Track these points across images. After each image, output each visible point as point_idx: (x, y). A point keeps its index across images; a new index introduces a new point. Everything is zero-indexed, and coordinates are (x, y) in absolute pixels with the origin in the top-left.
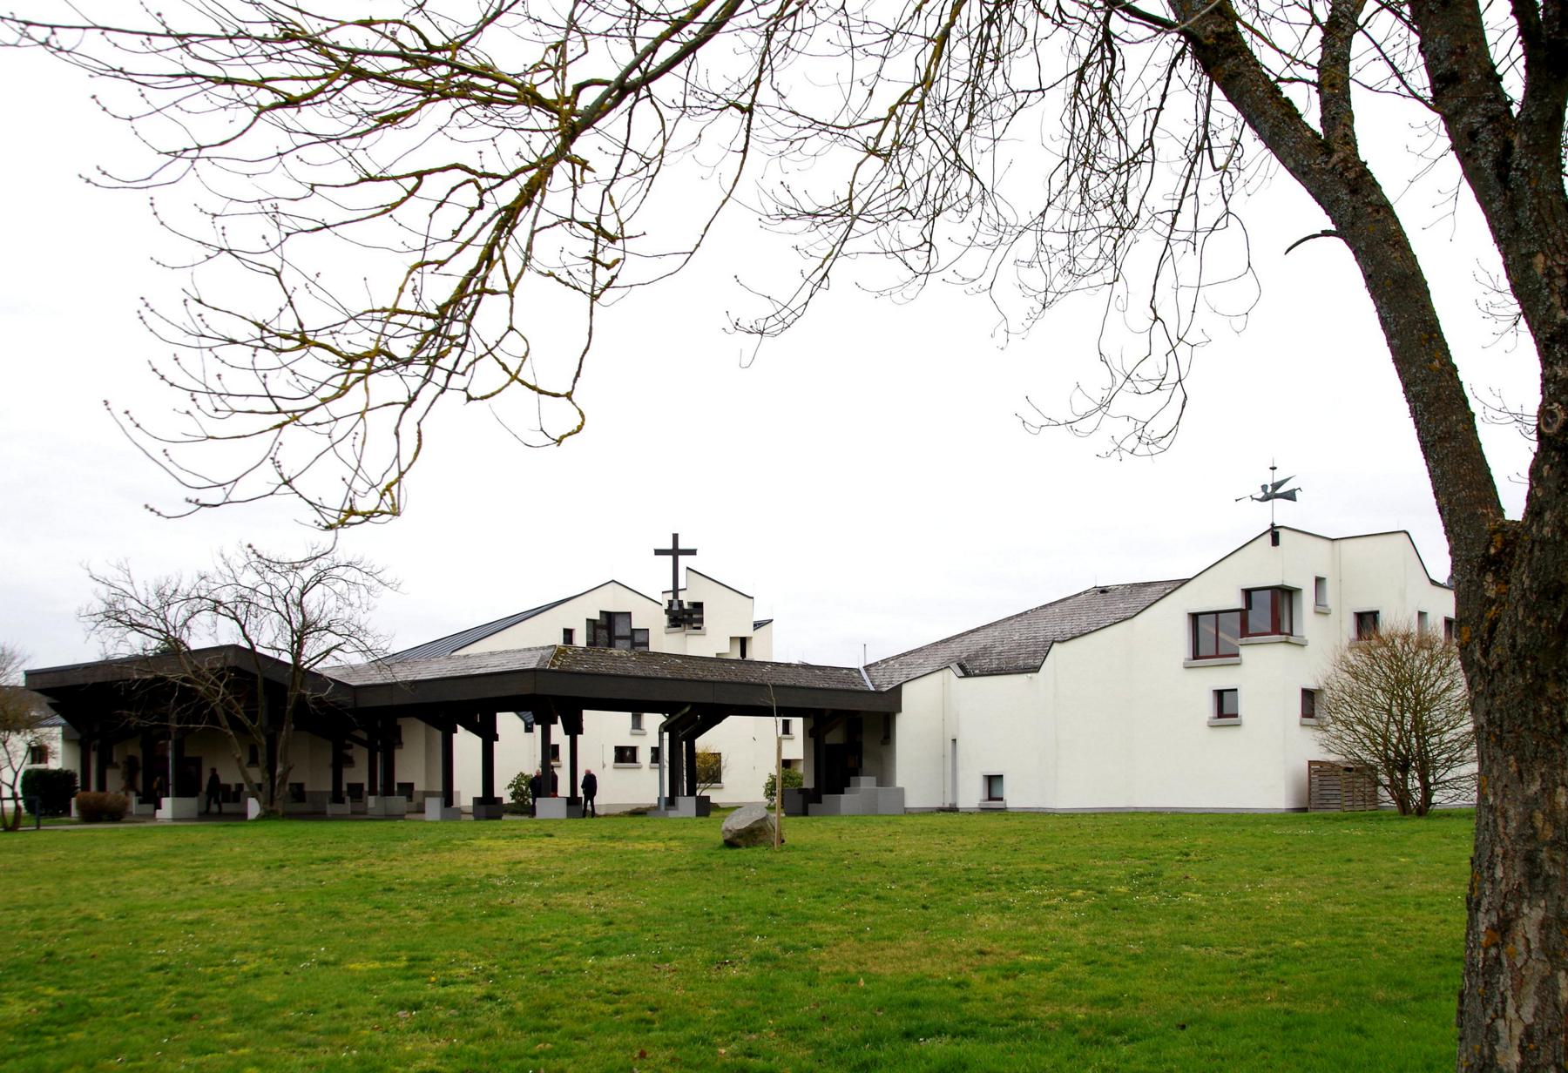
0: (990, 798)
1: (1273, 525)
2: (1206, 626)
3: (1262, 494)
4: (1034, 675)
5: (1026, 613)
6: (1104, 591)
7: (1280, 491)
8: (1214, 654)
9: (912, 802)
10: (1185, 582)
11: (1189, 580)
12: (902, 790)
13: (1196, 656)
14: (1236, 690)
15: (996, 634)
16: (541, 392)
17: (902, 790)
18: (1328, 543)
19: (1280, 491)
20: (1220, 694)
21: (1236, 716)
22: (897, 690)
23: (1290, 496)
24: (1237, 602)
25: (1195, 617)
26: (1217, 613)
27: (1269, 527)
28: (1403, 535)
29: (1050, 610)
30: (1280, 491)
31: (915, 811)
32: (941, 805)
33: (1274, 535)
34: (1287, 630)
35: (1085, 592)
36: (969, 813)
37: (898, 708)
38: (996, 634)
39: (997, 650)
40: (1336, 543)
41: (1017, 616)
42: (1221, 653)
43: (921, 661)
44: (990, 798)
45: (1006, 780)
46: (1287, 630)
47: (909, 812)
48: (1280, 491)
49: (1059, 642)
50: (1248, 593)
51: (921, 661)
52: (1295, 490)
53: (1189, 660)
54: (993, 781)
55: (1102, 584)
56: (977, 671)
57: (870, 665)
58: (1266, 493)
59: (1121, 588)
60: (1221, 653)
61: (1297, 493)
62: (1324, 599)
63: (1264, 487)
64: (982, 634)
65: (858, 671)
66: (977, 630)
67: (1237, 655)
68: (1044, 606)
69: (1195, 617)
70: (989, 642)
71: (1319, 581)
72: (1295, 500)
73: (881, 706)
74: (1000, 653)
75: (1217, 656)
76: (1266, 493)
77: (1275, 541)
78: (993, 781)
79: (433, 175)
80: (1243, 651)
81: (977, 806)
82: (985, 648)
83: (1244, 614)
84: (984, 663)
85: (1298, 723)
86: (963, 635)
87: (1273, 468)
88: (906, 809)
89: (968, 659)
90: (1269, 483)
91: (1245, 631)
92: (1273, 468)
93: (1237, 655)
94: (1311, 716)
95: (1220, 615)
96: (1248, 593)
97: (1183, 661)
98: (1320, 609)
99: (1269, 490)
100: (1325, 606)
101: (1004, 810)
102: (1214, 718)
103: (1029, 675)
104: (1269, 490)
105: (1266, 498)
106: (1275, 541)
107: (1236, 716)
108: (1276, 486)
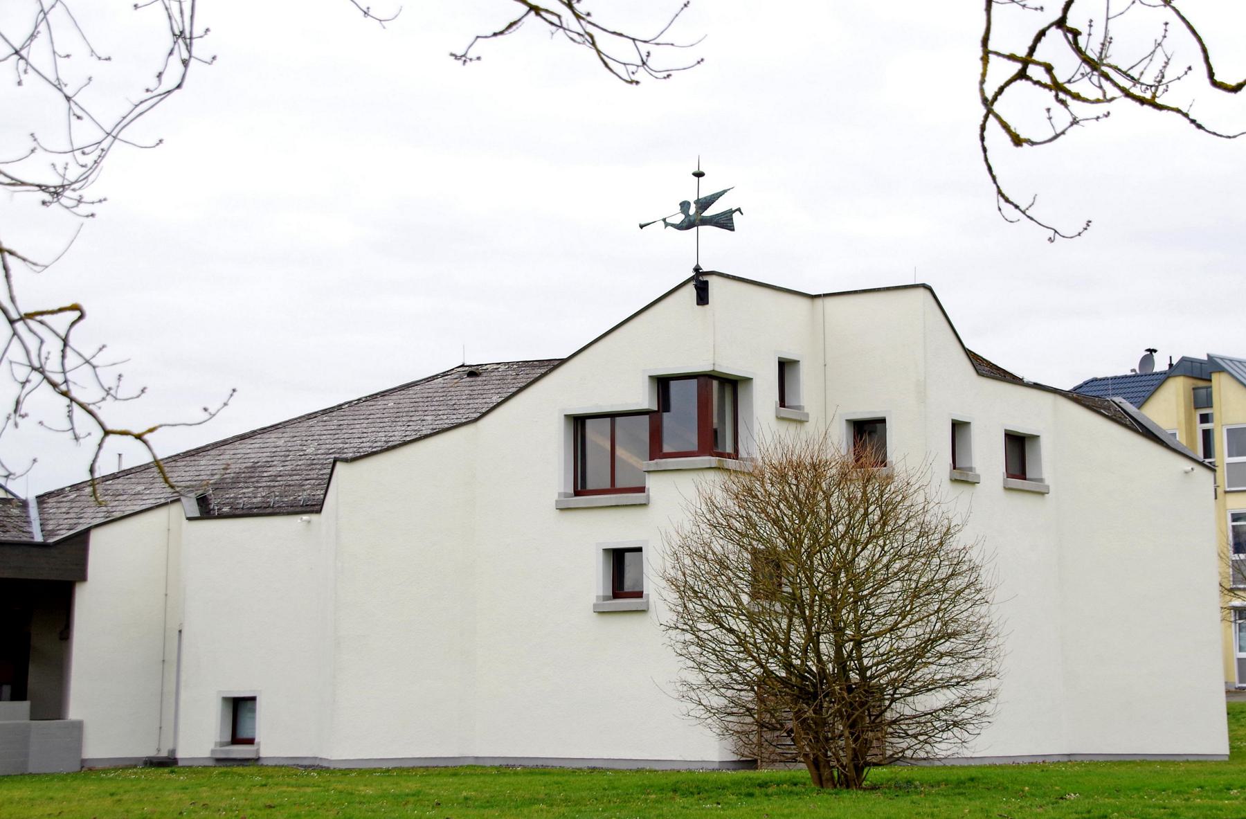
0: (236, 740)
1: (697, 269)
2: (596, 436)
3: (679, 219)
4: (314, 517)
5: (340, 407)
6: (473, 372)
7: (709, 212)
8: (608, 486)
9: (95, 748)
10: (553, 365)
11: (562, 362)
12: (78, 726)
13: (580, 489)
14: (639, 550)
15: (281, 442)
16: (1186, 115)
17: (78, 726)
18: (804, 302)
19: (709, 212)
20: (618, 558)
21: (639, 595)
22: (80, 541)
23: (725, 222)
24: (643, 398)
25: (578, 422)
26: (612, 416)
27: (692, 274)
28: (923, 293)
29: (381, 402)
30: (709, 212)
31: (99, 766)
32: (149, 752)
33: (701, 284)
34: (729, 449)
35: (444, 374)
36: (196, 769)
37: (81, 575)
38: (281, 442)
39: (273, 471)
40: (819, 302)
41: (325, 412)
42: (618, 485)
43: (140, 488)
44: (236, 740)
45: (260, 704)
46: (729, 449)
47: (88, 770)
48: (709, 212)
49: (346, 460)
50: (662, 384)
51: (140, 488)
52: (731, 212)
53: (566, 495)
54: (239, 707)
55: (472, 360)
56: (226, 509)
57: (49, 495)
58: (687, 215)
59: (503, 368)
60: (618, 485)
61: (736, 216)
62: (797, 394)
63: (685, 206)
64: (257, 442)
65: (24, 504)
66: (252, 434)
67: (642, 490)
68: (373, 397)
69: (578, 422)
70: (264, 457)
71: (785, 367)
72: (733, 230)
73: (43, 570)
74: (274, 478)
75: (613, 490)
76: (687, 215)
77: (703, 297)
78: (239, 707)
79: (1184, 16)
80: (652, 482)
81: (207, 754)
82: (254, 467)
83: (655, 418)
84: (246, 495)
85: (1001, 484)
86: (225, 443)
87: (699, 175)
88: (83, 761)
89: (219, 487)
90: (692, 199)
91: (656, 451)
92: (699, 175)
93: (642, 490)
94: (1022, 475)
95: (618, 419)
96: (662, 384)
97: (556, 497)
98: (785, 412)
99: (692, 211)
100: (798, 408)
101: (257, 760)
102: (606, 598)
103: (305, 517)
104: (692, 211)
105: (687, 225)
106: (703, 297)
107: (639, 595)
108: (704, 204)
